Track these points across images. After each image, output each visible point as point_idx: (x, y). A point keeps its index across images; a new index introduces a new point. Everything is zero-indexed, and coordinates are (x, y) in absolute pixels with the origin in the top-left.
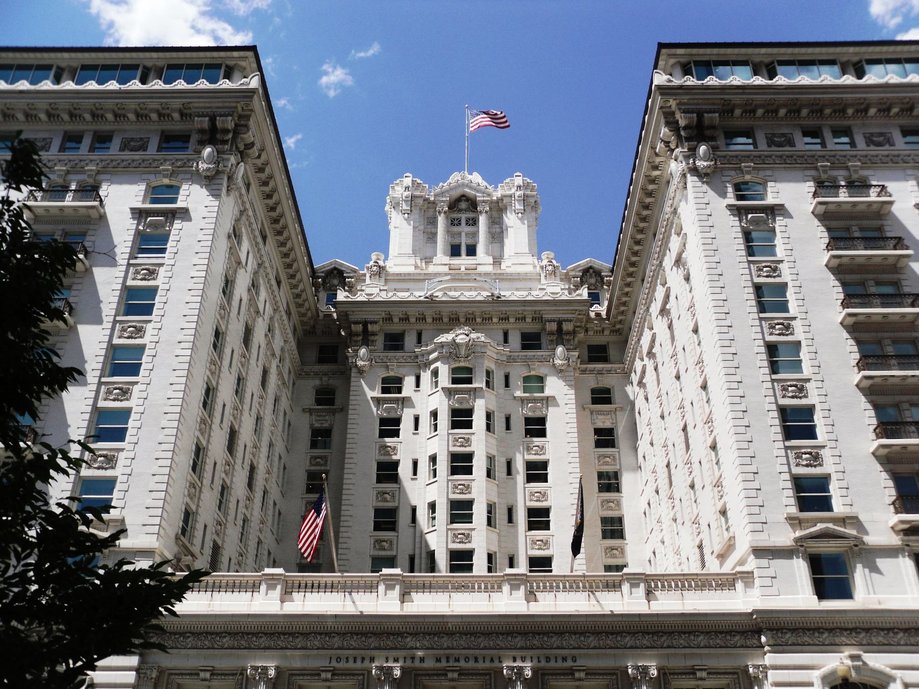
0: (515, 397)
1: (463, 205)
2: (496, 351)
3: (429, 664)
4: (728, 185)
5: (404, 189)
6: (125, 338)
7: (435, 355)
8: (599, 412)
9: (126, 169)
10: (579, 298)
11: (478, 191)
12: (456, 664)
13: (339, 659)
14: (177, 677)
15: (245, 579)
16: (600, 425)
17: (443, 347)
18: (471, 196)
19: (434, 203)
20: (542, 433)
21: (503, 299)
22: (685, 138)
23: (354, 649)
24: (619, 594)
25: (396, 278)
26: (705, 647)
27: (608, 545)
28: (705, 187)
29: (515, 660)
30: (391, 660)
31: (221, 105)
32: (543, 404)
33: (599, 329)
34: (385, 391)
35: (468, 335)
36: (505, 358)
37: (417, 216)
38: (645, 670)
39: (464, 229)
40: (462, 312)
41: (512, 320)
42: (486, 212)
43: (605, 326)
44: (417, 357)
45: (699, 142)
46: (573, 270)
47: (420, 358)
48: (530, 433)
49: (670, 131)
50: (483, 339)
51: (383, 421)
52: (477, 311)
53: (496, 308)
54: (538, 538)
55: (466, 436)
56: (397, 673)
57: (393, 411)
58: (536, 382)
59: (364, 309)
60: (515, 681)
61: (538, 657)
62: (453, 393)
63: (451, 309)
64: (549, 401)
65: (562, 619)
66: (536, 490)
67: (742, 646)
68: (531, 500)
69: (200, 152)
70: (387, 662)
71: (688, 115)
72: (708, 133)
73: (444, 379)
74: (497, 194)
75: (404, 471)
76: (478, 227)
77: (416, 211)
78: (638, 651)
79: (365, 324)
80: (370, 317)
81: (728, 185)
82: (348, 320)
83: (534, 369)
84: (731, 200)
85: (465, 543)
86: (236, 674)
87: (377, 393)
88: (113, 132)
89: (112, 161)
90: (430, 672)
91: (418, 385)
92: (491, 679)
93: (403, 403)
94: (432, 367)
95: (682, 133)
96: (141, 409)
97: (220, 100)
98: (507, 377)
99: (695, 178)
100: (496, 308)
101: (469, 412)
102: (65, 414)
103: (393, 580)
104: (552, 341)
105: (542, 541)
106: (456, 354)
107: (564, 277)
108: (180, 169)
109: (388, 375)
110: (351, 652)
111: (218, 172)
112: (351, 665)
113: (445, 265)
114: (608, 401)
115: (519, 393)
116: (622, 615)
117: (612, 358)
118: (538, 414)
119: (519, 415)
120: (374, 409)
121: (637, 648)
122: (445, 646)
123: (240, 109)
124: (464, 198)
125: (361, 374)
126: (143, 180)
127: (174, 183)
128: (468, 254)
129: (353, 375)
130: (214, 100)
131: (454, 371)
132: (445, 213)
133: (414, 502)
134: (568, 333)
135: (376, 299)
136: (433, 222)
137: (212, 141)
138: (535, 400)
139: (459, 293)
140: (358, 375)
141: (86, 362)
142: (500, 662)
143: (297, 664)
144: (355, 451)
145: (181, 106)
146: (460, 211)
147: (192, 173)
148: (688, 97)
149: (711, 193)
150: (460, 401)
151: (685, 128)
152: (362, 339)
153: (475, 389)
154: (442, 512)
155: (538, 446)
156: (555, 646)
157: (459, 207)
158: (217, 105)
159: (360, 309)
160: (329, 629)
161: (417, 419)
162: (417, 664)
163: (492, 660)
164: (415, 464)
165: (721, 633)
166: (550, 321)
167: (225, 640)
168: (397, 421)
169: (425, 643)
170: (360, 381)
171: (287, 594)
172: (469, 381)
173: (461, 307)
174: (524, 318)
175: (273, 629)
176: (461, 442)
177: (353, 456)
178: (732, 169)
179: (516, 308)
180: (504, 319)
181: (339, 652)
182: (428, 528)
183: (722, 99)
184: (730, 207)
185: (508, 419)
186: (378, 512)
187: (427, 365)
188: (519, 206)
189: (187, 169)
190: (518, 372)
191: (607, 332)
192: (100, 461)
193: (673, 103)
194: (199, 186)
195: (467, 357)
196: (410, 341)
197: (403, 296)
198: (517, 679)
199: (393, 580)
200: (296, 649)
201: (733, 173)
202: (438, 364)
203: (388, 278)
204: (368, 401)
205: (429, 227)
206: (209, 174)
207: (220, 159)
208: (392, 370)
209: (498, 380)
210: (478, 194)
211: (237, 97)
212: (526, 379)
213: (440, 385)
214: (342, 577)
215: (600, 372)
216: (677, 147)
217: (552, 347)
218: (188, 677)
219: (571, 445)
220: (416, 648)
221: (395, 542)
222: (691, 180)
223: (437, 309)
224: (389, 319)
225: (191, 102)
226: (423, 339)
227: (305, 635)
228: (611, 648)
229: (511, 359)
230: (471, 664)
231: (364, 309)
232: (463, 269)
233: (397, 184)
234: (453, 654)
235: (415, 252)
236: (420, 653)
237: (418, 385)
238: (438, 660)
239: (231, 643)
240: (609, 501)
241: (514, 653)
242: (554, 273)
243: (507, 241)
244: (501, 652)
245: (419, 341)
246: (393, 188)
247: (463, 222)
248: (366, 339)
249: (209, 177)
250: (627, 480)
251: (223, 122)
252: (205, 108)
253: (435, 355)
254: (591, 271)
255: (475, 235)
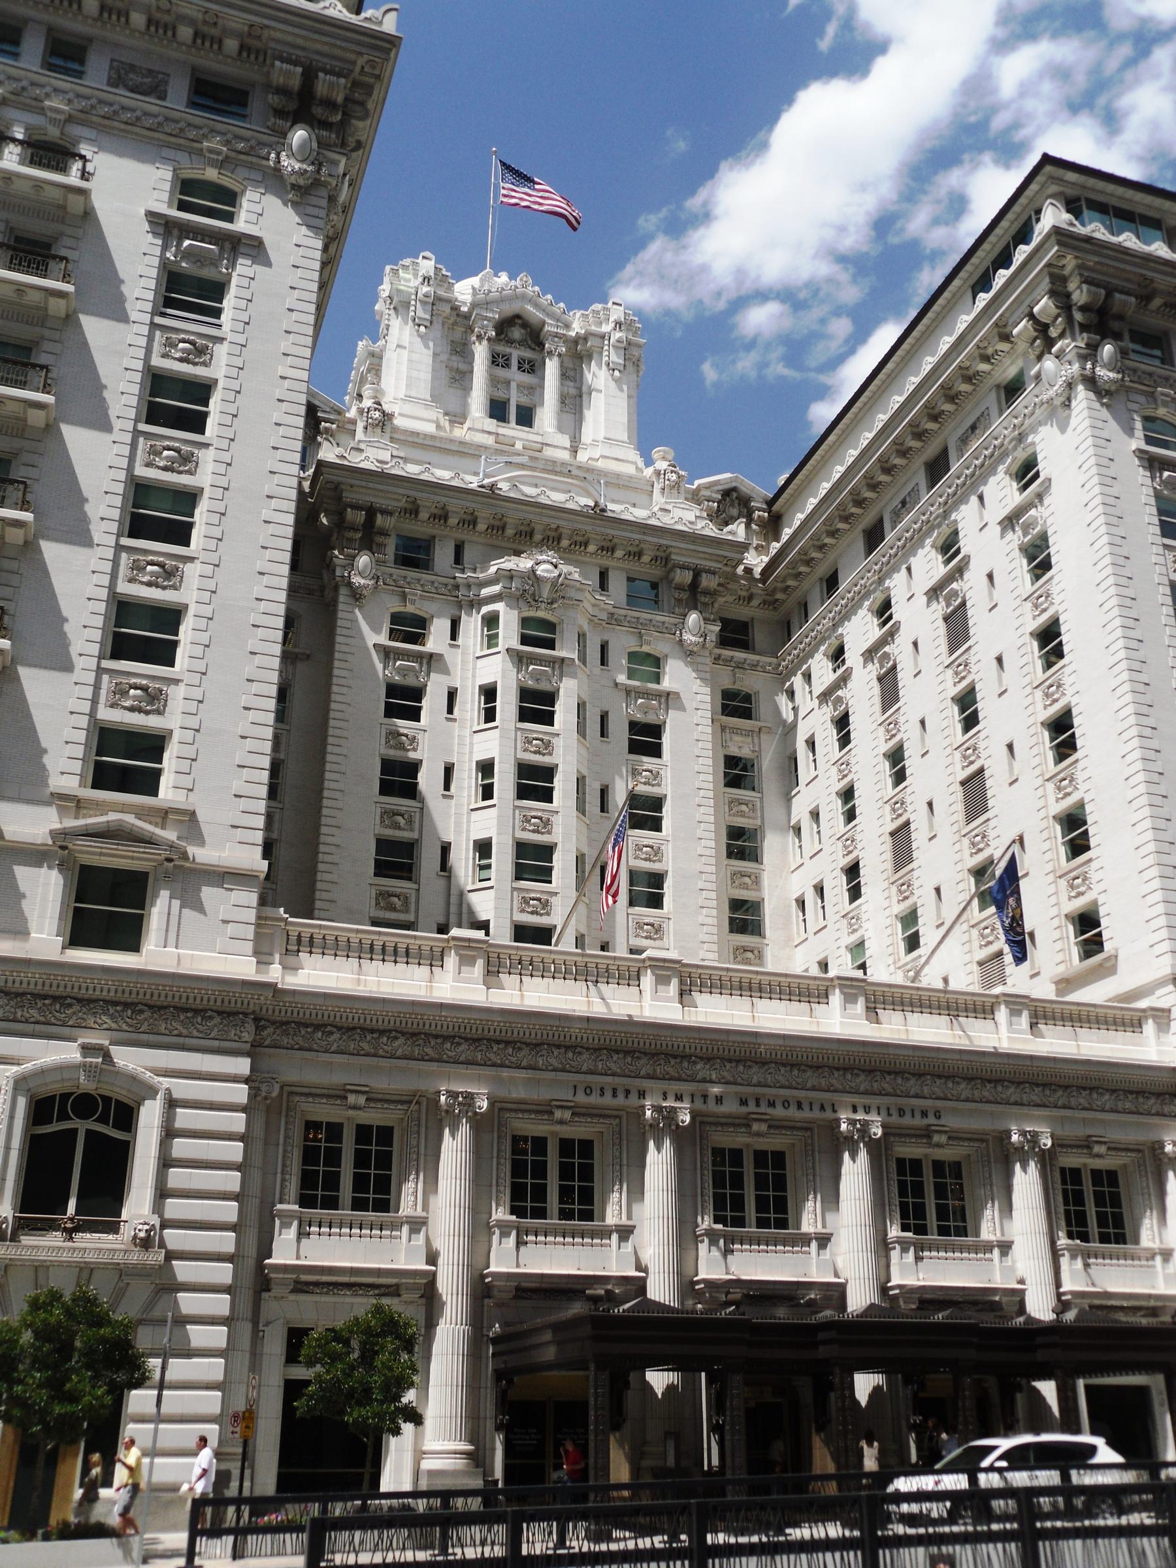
0: (616, 685)
1: (517, 333)
2: (593, 601)
3: (730, 1107)
4: (1136, 417)
5: (420, 279)
6: (159, 467)
7: (496, 589)
8: (735, 731)
9: (129, 128)
10: (730, 538)
11: (548, 315)
12: (770, 1111)
13: (588, 1091)
14: (303, 1099)
15: (418, 942)
16: (734, 751)
17: (511, 578)
18: (533, 321)
19: (467, 316)
20: (655, 751)
21: (610, 514)
22: (1081, 325)
23: (613, 1075)
24: (989, 1024)
25: (410, 439)
26: (1112, 1111)
27: (738, 944)
28: (1105, 413)
29: (855, 1110)
30: (671, 1097)
31: (326, 49)
32: (660, 703)
33: (744, 593)
34: (393, 634)
35: (556, 567)
36: (604, 616)
37: (439, 335)
38: (1034, 1138)
39: (515, 375)
40: (540, 522)
41: (619, 553)
42: (560, 355)
43: (754, 590)
44: (457, 587)
45: (1103, 338)
46: (709, 486)
47: (463, 591)
48: (636, 748)
49: (1057, 307)
50: (576, 576)
51: (393, 690)
52: (566, 526)
53: (598, 529)
54: (647, 920)
55: (546, 738)
56: (685, 1118)
57: (411, 674)
58: (651, 664)
59: (371, 485)
60: (857, 1142)
61: (888, 1109)
62: (392, 656)
63: (526, 516)
64: (668, 699)
65: (927, 1054)
66: (646, 842)
67: (1158, 1114)
68: (636, 858)
69: (284, 135)
70: (665, 1099)
71: (1093, 289)
72: (1115, 325)
73: (509, 632)
74: (577, 327)
75: (428, 780)
76: (543, 379)
77: (437, 326)
78: (1025, 1110)
79: (371, 512)
80: (382, 501)
81: (1136, 417)
82: (340, 498)
83: (649, 643)
84: (1137, 442)
85: (541, 915)
86: (410, 1102)
87: (383, 639)
88: (90, 40)
89: (101, 102)
90: (723, 1120)
91: (454, 636)
92: (812, 1136)
93: (429, 663)
94: (485, 609)
95: (1078, 316)
96: (207, 611)
97: (328, 39)
98: (604, 648)
99: (1091, 395)
100: (598, 529)
101: (550, 698)
102: (54, 596)
103: (668, 968)
104: (679, 601)
105: (652, 925)
106: (533, 595)
107: (690, 496)
108: (243, 157)
109: (402, 609)
110: (609, 1079)
111: (317, 183)
112: (608, 1100)
113: (489, 433)
114: (747, 714)
115: (622, 678)
116: (1008, 1055)
117: (758, 646)
118: (651, 719)
119: (623, 713)
120: (379, 666)
121: (1022, 1104)
122: (755, 1081)
123: (358, 69)
124: (520, 321)
125: (357, 600)
126: (166, 160)
127: (227, 182)
128: (520, 422)
129: (341, 599)
130: (316, 36)
131: (525, 622)
132: (489, 339)
133: (448, 836)
134: (707, 592)
135: (393, 472)
136: (462, 350)
137: (300, 116)
138: (647, 695)
139: (538, 491)
140: (352, 601)
141: (87, 500)
142: (835, 1111)
143: (519, 1093)
144: (345, 734)
145: (246, 28)
146: (511, 342)
147: (264, 171)
148: (1096, 259)
149: (1113, 426)
150: (537, 676)
151: (1083, 309)
152: (361, 538)
153: (563, 660)
154: (503, 859)
155: (651, 771)
156: (912, 1093)
157: (510, 334)
158: (318, 47)
159: (364, 484)
160: (573, 1038)
161: (452, 695)
162: (712, 1106)
163: (822, 1108)
164: (449, 770)
165: (1131, 1092)
166: (683, 567)
167: (396, 1043)
168: (417, 694)
169: (725, 1074)
170: (352, 612)
171: (492, 973)
172: (550, 644)
173: (541, 514)
174: (639, 554)
175: (480, 1031)
176: (536, 746)
177: (342, 742)
178: (1143, 393)
179: (603, 530)
180: (609, 549)
181: (590, 1078)
182: (473, 883)
183: (1142, 275)
184: (1140, 453)
185: (604, 718)
186: (383, 845)
187: (475, 604)
188: (616, 358)
189: (254, 160)
190: (622, 643)
191: (755, 602)
192: (134, 696)
193: (1070, 262)
194: (279, 202)
195: (552, 603)
196: (443, 556)
197: (443, 475)
198: (862, 1138)
199: (668, 968)
200: (519, 1067)
201: (1142, 399)
202: (499, 607)
203: (396, 436)
204: (367, 649)
205: (454, 358)
206: (301, 182)
207: (321, 159)
208: (413, 602)
209: (594, 653)
210: (549, 321)
211: (359, 43)
212: (633, 657)
213: (502, 644)
214: (583, 955)
215: (740, 666)
216: (1062, 336)
217: (681, 610)
218: (324, 1101)
219: (702, 777)
220: (711, 1082)
221: (413, 899)
222: (1082, 395)
223: (499, 510)
224: (413, 511)
225: (267, 27)
226: (468, 555)
227: (535, 1046)
228: (988, 1102)
229: (613, 619)
230: (793, 1112)
231: (371, 485)
232: (519, 446)
233: (405, 267)
234: (764, 1095)
235: (436, 398)
236: (716, 1090)
237: (454, 636)
238: (744, 1102)
239: (407, 1050)
240: (743, 875)
241: (856, 1099)
242: (676, 486)
243: (589, 415)
244: (836, 1097)
245: (458, 559)
246: (395, 272)
247: (514, 363)
248: (369, 538)
249: (300, 187)
250: (772, 845)
251: (331, 85)
252: (294, 46)
253: (496, 589)
254: (735, 495)
255: (536, 390)
